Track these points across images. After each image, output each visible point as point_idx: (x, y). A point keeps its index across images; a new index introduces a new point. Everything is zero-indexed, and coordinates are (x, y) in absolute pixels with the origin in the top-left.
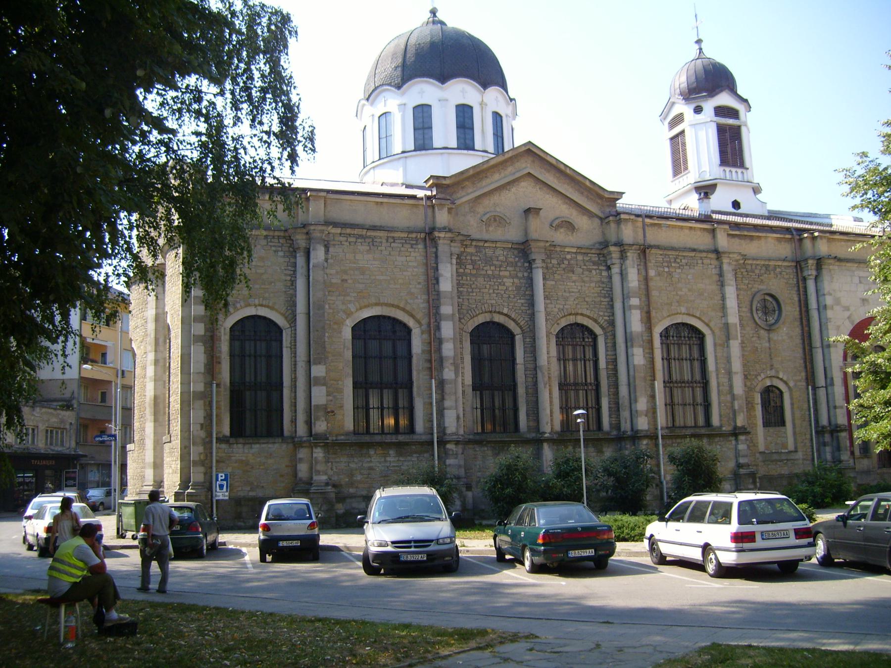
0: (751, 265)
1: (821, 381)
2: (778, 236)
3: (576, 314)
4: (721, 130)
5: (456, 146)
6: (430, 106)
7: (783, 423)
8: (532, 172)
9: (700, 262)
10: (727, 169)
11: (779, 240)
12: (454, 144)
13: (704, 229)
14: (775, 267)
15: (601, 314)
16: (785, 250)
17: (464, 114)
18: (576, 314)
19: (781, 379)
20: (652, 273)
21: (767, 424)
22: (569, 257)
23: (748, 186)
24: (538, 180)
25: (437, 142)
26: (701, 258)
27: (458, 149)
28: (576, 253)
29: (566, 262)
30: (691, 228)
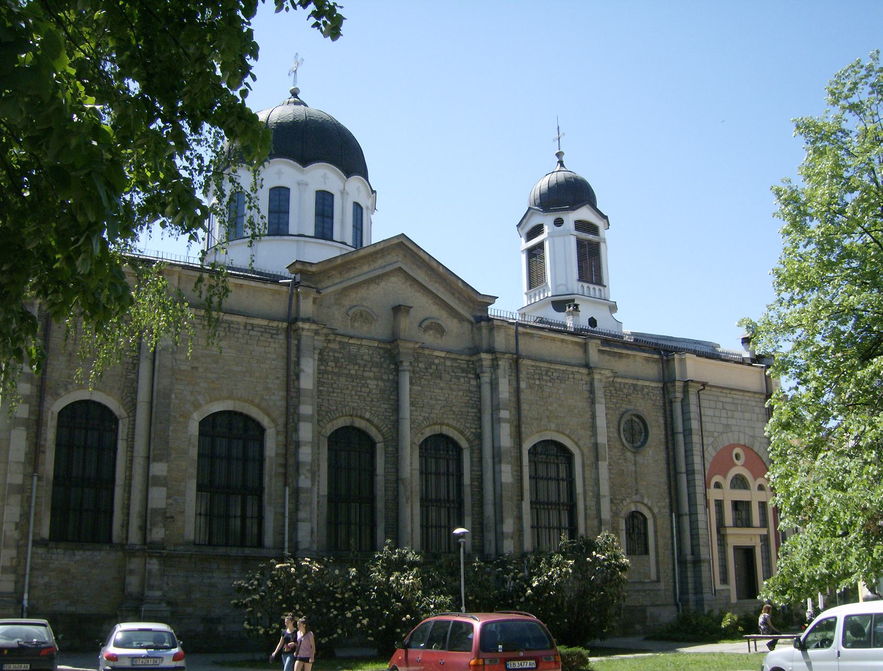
0: (620, 383)
3: (442, 424)
5: (313, 235)
6: (288, 189)
7: (646, 552)
8: (403, 267)
10: (586, 285)
12: (311, 231)
15: (469, 425)
22: (437, 361)
26: (573, 373)
29: (434, 367)
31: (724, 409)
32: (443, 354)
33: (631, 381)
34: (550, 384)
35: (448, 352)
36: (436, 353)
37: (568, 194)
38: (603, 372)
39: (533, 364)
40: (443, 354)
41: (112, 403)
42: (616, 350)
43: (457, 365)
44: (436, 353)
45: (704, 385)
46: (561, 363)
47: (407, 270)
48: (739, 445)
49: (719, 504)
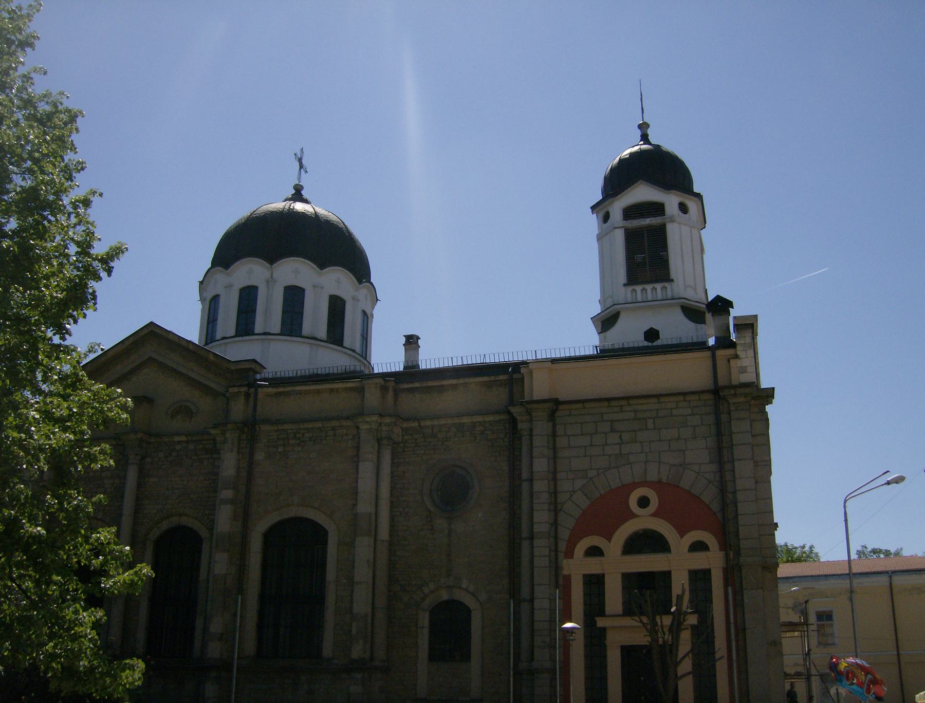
0: (433, 427)
1: (525, 592)
2: (486, 379)
3: (180, 515)
4: (632, 237)
5: (278, 330)
6: (303, 290)
7: (467, 657)
8: (155, 356)
9: (331, 433)
10: (639, 288)
11: (488, 385)
12: (277, 328)
13: (351, 389)
14: (474, 425)
15: (207, 512)
16: (498, 397)
17: (294, 297)
18: (180, 515)
19: (466, 590)
20: (259, 456)
21: (434, 656)
22: (178, 447)
23: (670, 305)
24: (162, 366)
25: (307, 329)
26: (333, 429)
27: (236, 336)
28: (187, 442)
29: (174, 454)
30: (332, 390)
31: (613, 430)
32: (184, 438)
33: (457, 421)
34: (300, 449)
35: (186, 436)
36: (177, 439)
37: (657, 167)
38: (368, 419)
39: (276, 428)
40: (184, 438)
41: (196, 525)
42: (430, 384)
43: (201, 446)
44: (177, 439)
45: (557, 402)
46: (316, 420)
47: (160, 359)
48: (645, 484)
49: (595, 583)
